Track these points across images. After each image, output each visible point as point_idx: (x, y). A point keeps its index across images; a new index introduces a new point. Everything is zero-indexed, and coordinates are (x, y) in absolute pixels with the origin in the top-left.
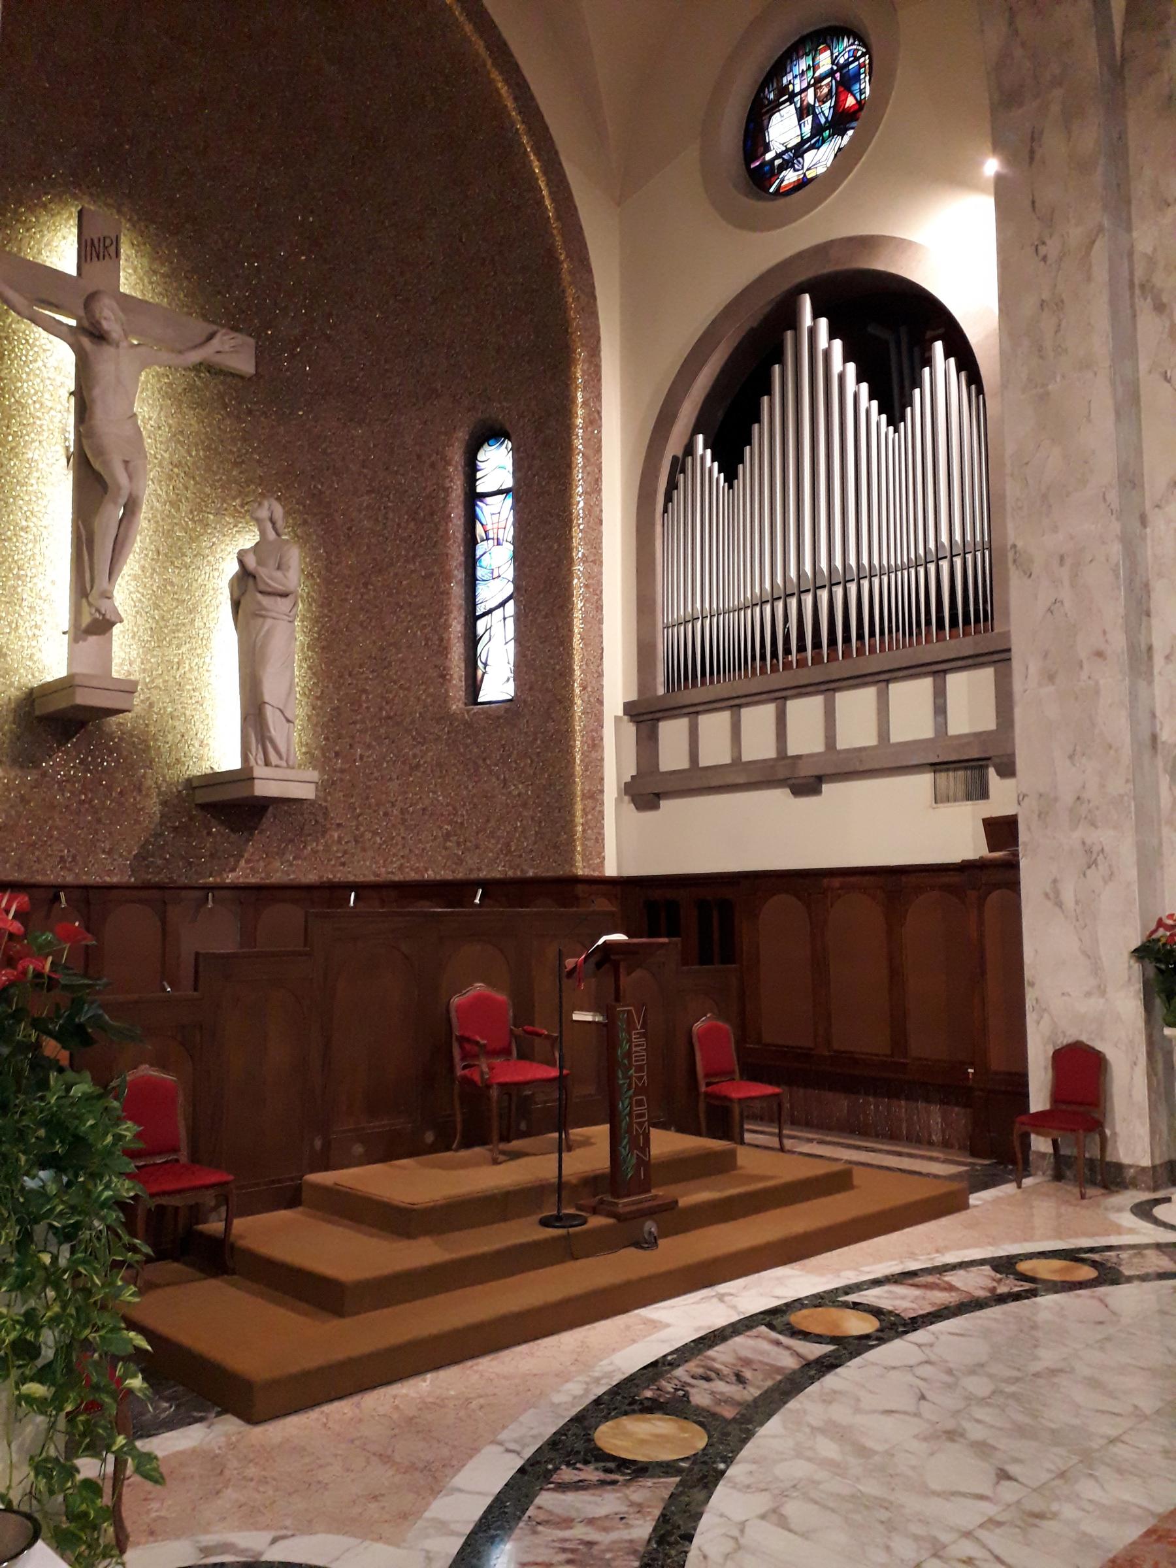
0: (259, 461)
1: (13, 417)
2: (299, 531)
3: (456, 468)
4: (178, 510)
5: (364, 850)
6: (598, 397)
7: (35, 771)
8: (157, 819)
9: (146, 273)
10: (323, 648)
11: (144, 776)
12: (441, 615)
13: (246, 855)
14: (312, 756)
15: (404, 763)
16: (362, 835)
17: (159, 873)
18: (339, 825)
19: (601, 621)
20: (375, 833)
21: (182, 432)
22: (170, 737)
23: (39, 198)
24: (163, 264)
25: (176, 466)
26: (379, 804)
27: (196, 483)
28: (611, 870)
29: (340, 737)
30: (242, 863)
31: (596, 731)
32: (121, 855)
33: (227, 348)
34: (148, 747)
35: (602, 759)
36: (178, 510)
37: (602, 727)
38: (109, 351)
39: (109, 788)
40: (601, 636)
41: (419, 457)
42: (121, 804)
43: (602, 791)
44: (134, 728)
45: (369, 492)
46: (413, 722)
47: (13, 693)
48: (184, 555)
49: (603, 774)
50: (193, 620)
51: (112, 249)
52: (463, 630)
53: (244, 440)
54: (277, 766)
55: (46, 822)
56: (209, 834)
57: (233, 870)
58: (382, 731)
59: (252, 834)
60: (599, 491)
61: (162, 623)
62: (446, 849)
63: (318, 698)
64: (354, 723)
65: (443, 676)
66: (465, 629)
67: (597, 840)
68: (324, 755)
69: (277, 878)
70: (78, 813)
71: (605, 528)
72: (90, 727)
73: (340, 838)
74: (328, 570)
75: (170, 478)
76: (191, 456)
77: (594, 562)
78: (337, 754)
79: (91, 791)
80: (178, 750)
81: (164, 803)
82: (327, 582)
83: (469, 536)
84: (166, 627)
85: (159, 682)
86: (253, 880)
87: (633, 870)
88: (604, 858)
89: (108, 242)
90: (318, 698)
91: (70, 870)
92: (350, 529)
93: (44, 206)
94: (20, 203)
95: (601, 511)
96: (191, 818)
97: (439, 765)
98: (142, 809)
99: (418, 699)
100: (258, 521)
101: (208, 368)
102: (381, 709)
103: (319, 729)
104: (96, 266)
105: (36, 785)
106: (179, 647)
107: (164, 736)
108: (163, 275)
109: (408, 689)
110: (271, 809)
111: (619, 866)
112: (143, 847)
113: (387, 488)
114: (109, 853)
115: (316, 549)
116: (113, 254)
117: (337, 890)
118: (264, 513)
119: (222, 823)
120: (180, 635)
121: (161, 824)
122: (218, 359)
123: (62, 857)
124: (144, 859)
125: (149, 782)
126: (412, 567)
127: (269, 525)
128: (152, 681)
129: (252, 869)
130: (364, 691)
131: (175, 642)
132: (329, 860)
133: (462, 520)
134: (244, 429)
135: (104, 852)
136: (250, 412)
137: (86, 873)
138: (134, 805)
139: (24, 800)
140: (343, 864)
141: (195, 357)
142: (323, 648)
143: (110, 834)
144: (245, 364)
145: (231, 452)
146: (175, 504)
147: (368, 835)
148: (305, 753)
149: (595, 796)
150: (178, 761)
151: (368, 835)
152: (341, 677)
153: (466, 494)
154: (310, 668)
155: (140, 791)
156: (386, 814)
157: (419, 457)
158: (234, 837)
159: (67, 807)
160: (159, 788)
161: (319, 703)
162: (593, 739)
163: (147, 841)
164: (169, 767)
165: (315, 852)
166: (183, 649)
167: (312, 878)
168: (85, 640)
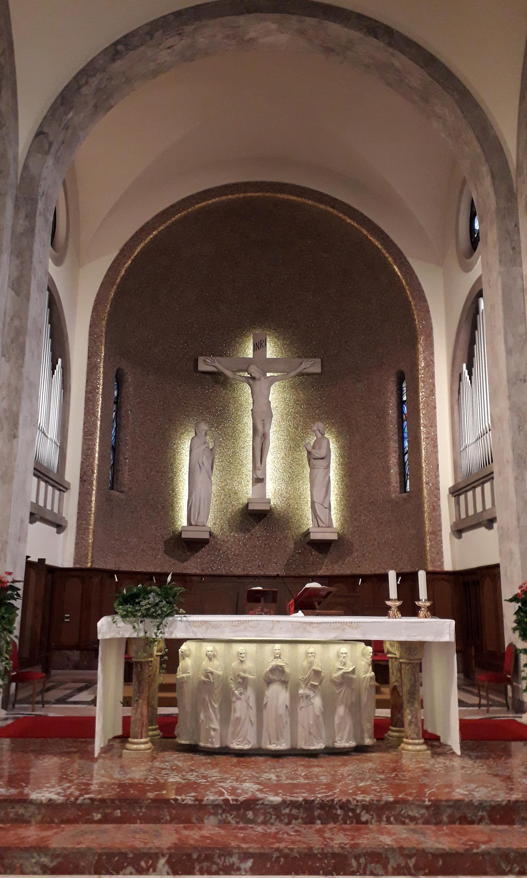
0: (325, 405)
1: (238, 410)
2: (340, 430)
3: (392, 393)
4: (297, 430)
5: (366, 560)
6: (432, 354)
7: (249, 534)
8: (292, 550)
9: (282, 346)
10: (349, 476)
11: (288, 533)
12: (388, 456)
13: (325, 563)
14: (347, 521)
15: (378, 521)
16: (365, 554)
17: (294, 571)
18: (357, 550)
19: (437, 452)
20: (369, 553)
21: (298, 401)
22: (296, 517)
23: (242, 333)
24: (287, 341)
25: (296, 414)
26: (370, 540)
27: (304, 418)
28: (448, 567)
29: (356, 512)
30: (324, 567)
31: (436, 502)
32: (280, 564)
33: (308, 366)
34: (289, 522)
35: (440, 516)
36: (297, 430)
37: (439, 500)
38: (258, 382)
39: (275, 538)
40: (437, 459)
41: (379, 391)
42: (280, 545)
43: (440, 530)
44: (284, 515)
45: (363, 409)
46: (380, 504)
47: (241, 506)
48: (300, 446)
49: (441, 522)
50: (303, 471)
51: (264, 344)
52: (398, 461)
53: (320, 398)
54: (322, 527)
55: (253, 552)
56: (312, 554)
57: (320, 569)
58: (370, 508)
59: (327, 555)
60: (434, 395)
61: (293, 474)
62: (393, 559)
63: (348, 496)
64: (361, 505)
65: (389, 483)
66: (399, 460)
67: (438, 554)
68: (351, 520)
69: (336, 573)
70: (265, 548)
71: (438, 410)
72: (268, 516)
73: (358, 555)
74: (350, 443)
75: (295, 418)
76: (301, 408)
77: (431, 426)
78: (355, 519)
79: (269, 540)
80: (300, 522)
81: (295, 543)
82: (350, 448)
83: (400, 420)
84: (294, 475)
85: (292, 496)
86: (327, 574)
87: (460, 567)
88: (443, 562)
89: (262, 342)
90: (348, 496)
91: (262, 570)
92: (357, 425)
93: (244, 335)
94: (236, 337)
95: (435, 403)
96: (305, 549)
97: (389, 521)
98: (287, 546)
99: (382, 493)
100: (314, 431)
101: (301, 374)
102: (370, 499)
103: (349, 509)
104: (258, 351)
105: (249, 539)
106: (299, 482)
107: (294, 517)
108: (288, 345)
109: (378, 489)
110: (333, 544)
111: (453, 563)
112: (288, 561)
113: (369, 406)
114: (276, 563)
115: (346, 436)
116: (264, 346)
117: (356, 577)
118: (315, 428)
119: (316, 550)
120: (299, 477)
121: (294, 551)
122: (305, 371)
123: (259, 565)
124: (289, 565)
125: (289, 535)
126: (378, 437)
127: (318, 432)
128: (290, 496)
129: (327, 569)
130: (364, 492)
131: (298, 480)
132: (354, 565)
133: (396, 414)
134: (320, 394)
135: (274, 563)
136: (322, 387)
137: (268, 571)
138: (285, 544)
139: (245, 545)
140: (359, 567)
141: (293, 374)
142: (349, 476)
143: (276, 556)
144: (317, 369)
145: (316, 404)
146: (296, 428)
147: (367, 554)
148: (344, 520)
149: (437, 533)
150: (300, 526)
151: (367, 554)
152: (356, 486)
153: (398, 402)
154: (345, 484)
155: (286, 538)
156: (373, 544)
157: (379, 391)
158: (321, 556)
159: (261, 546)
160: (293, 537)
161: (348, 498)
162: (434, 507)
163: (290, 559)
164: (297, 529)
165: (349, 561)
166: (300, 483)
167: (348, 572)
168: (256, 485)
